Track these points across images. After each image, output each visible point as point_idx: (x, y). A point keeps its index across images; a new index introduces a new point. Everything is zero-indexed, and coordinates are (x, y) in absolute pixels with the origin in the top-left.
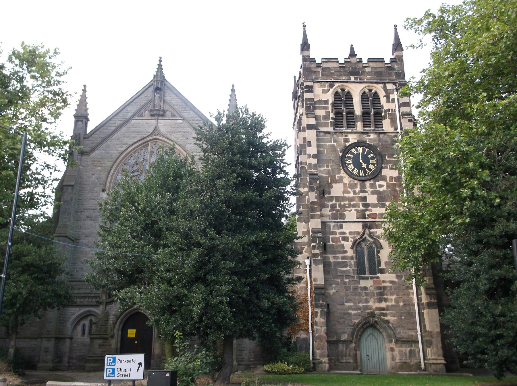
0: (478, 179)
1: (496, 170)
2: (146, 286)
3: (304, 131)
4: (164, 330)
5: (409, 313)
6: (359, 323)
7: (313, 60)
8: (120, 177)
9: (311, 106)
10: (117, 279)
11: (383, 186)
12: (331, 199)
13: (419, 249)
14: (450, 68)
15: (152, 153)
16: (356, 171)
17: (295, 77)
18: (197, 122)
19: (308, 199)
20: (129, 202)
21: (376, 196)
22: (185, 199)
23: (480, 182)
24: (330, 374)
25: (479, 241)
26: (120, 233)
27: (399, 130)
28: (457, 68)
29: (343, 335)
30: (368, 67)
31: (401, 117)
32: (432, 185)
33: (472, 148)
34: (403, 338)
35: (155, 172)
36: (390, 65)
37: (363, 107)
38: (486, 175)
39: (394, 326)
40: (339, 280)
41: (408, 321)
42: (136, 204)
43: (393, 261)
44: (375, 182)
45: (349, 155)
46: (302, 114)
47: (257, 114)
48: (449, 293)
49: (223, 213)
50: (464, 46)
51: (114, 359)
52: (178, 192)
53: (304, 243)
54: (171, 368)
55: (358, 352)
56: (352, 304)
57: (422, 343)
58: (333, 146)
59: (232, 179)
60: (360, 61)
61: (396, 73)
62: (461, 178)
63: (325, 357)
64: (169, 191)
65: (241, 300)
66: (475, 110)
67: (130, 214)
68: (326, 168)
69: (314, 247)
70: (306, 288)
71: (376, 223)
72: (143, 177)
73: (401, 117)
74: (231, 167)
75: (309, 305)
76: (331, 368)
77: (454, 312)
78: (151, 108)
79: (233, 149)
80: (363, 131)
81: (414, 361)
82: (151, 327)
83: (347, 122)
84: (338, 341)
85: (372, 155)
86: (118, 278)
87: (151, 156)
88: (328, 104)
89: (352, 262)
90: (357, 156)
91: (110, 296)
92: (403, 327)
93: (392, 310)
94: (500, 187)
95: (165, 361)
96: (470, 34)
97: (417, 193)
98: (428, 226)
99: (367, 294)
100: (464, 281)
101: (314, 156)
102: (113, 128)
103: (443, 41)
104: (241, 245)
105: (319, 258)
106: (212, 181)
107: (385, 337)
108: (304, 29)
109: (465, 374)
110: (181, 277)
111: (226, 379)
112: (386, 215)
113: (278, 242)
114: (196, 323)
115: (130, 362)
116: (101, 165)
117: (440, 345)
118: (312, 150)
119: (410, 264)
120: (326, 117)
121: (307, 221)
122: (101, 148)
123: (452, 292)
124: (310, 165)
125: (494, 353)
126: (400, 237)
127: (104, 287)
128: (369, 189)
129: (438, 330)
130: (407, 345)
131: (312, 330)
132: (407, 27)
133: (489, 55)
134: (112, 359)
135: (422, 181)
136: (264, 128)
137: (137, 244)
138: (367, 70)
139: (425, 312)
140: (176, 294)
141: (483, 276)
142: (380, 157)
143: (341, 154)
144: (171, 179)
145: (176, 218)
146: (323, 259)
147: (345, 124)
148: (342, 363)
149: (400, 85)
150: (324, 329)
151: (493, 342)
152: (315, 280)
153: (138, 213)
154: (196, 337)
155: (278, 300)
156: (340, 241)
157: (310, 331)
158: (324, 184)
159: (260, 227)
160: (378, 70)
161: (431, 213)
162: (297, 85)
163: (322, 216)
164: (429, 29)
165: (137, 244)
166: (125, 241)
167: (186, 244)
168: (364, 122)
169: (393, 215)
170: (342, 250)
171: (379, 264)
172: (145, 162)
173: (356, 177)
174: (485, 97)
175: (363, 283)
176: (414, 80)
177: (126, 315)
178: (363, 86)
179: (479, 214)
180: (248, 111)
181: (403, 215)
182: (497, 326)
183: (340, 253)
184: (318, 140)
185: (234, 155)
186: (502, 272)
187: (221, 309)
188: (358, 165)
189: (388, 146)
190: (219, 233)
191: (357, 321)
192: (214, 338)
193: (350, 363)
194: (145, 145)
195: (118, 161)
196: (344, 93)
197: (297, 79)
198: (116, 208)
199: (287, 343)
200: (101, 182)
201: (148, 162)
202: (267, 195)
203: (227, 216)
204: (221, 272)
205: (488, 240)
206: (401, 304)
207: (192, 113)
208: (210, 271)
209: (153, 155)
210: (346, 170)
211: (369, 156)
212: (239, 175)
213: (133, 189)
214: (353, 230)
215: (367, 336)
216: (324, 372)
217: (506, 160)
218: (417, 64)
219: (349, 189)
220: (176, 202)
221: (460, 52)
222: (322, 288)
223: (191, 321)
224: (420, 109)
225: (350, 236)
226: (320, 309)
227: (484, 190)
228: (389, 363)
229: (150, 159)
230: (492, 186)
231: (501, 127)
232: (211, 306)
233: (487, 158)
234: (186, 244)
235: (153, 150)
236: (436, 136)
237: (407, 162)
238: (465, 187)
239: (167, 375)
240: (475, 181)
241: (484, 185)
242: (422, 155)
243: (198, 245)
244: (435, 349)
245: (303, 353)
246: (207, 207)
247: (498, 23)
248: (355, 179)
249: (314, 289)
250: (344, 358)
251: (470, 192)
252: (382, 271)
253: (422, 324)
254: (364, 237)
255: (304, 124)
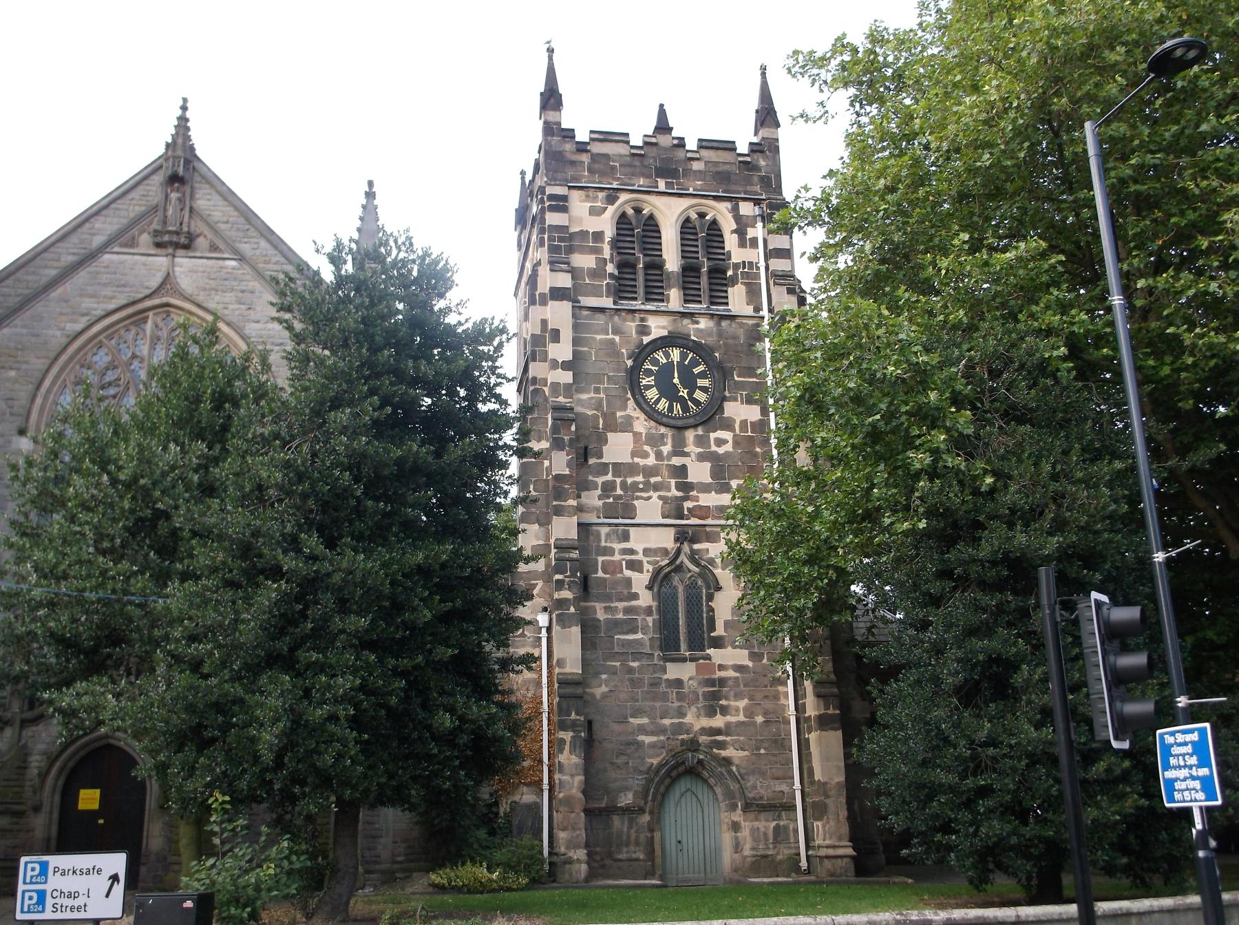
0: (948, 431)
1: (986, 412)
2: (132, 678)
3: (544, 303)
4: (179, 789)
5: (775, 741)
6: (661, 766)
7: (569, 134)
8: (69, 399)
9: (563, 245)
10: (53, 660)
11: (725, 442)
12: (603, 469)
13: (807, 590)
14: (889, 171)
15: (155, 340)
16: (663, 405)
17: (523, 173)
18: (276, 266)
19: (549, 469)
20: (93, 462)
21: (708, 465)
22: (243, 457)
23: (952, 436)
24: (591, 887)
25: (945, 574)
26: (65, 541)
27: (765, 312)
28: (904, 173)
29: (622, 795)
30: (698, 159)
31: (771, 283)
32: (843, 443)
33: (935, 359)
34: (761, 798)
35: (164, 387)
36: (748, 159)
37: (684, 254)
38: (964, 420)
39: (742, 771)
40: (618, 664)
41: (774, 759)
42: (112, 467)
43: (745, 618)
44: (708, 432)
45: (648, 366)
46: (539, 263)
47: (435, 253)
48: (875, 693)
49: (345, 494)
50: (923, 123)
51: (44, 866)
52: (223, 442)
53: (533, 575)
54: (198, 887)
55: (657, 835)
56: (645, 720)
57: (804, 811)
58: (612, 342)
59: (369, 410)
60: (681, 143)
61: (762, 179)
62: (909, 427)
63: (579, 847)
64: (200, 436)
65: (383, 712)
66: (943, 272)
67: (95, 492)
68: (592, 395)
69: (560, 585)
70: (538, 683)
71: (708, 529)
72: (130, 401)
73: (771, 283)
74: (367, 379)
75: (545, 722)
76: (592, 875)
77: (884, 736)
78: (155, 226)
79: (373, 335)
80: (682, 310)
81: (784, 853)
82: (142, 787)
83: (646, 287)
84: (612, 810)
85: (701, 368)
86: (57, 656)
87: (153, 347)
88: (602, 241)
89: (650, 619)
90: (667, 370)
91: (32, 703)
92: (763, 774)
93: (739, 735)
94: (994, 451)
95: (176, 867)
96: (937, 95)
97: (803, 458)
98: (828, 537)
99: (681, 697)
100: (908, 665)
101: (566, 366)
102: (53, 272)
103: (873, 110)
104: (387, 575)
105: (572, 610)
106: (317, 413)
107: (720, 797)
108: (550, 58)
109: (897, 879)
110: (229, 655)
111: (340, 909)
112: (732, 511)
113: (479, 570)
114: (265, 770)
115: (88, 873)
116: (17, 365)
117: (844, 813)
118: (562, 351)
119: (786, 626)
120: (597, 273)
121: (545, 522)
122: (18, 321)
123: (882, 691)
124: (555, 387)
125: (971, 830)
126: (763, 562)
127: (17, 680)
128: (692, 448)
129: (841, 778)
130: (770, 815)
131: (550, 783)
132: (793, 71)
133: (976, 148)
134: (37, 867)
135: (818, 432)
136: (450, 288)
137: (111, 569)
138: (696, 166)
139: (813, 737)
140: (214, 698)
141: (953, 653)
142: (720, 372)
143: (629, 363)
144: (206, 405)
145: (220, 505)
146: (582, 614)
147: (641, 291)
148: (620, 860)
149: (770, 206)
150: (580, 782)
151: (969, 804)
152: (561, 663)
153: (117, 490)
154: (265, 805)
155: (477, 711)
156: (621, 571)
157: (546, 787)
158: (587, 433)
159: (436, 532)
160: (720, 169)
161: (838, 506)
162: (528, 192)
163: (580, 509)
164: (844, 77)
165: (111, 569)
166: (80, 562)
167: (244, 572)
168: (684, 288)
169: (749, 512)
170: (625, 592)
171: (712, 627)
172: (136, 363)
173: (664, 420)
174: (964, 242)
175: (674, 671)
176: (809, 195)
177: (74, 754)
178: (685, 203)
179: (947, 510)
180: (411, 244)
181: (772, 511)
182: (978, 770)
183: (621, 600)
184: (576, 327)
185: (374, 350)
186: (994, 643)
187: (332, 735)
188: (668, 391)
189: (739, 348)
190: (331, 544)
191: (655, 761)
192: (311, 807)
193: (637, 860)
194: (139, 318)
195: (64, 358)
196: (640, 215)
197: (529, 177)
198: (56, 477)
199: (489, 817)
200: (15, 410)
201: (146, 363)
202: (455, 452)
203: (353, 502)
204: (333, 642)
205: (965, 571)
206: (760, 719)
207: (263, 244)
208: (305, 638)
209: (158, 347)
210: (641, 400)
211: (696, 371)
212: (385, 402)
213: (106, 430)
214: (653, 545)
215: (678, 794)
216: (576, 885)
217: (1008, 390)
218: (813, 158)
219: (647, 448)
220: (217, 465)
221: (910, 137)
222: (577, 684)
223: (254, 765)
224: (820, 263)
225: (645, 560)
226: (571, 734)
227: (959, 455)
228: (727, 857)
229: (151, 356)
230: (976, 448)
231: (998, 313)
232: (305, 726)
233: (967, 384)
234: (244, 572)
235: (160, 333)
236: (857, 326)
237: (789, 384)
238: (917, 448)
239: (185, 905)
240: (941, 433)
241: (960, 443)
242: (824, 370)
243: (276, 573)
244: (832, 823)
245: (527, 839)
246: (301, 477)
247: (999, 74)
248: (660, 424)
249: (556, 685)
250: (625, 849)
251: (928, 460)
252: (718, 643)
253: (805, 767)
254: (678, 562)
255: (544, 286)
